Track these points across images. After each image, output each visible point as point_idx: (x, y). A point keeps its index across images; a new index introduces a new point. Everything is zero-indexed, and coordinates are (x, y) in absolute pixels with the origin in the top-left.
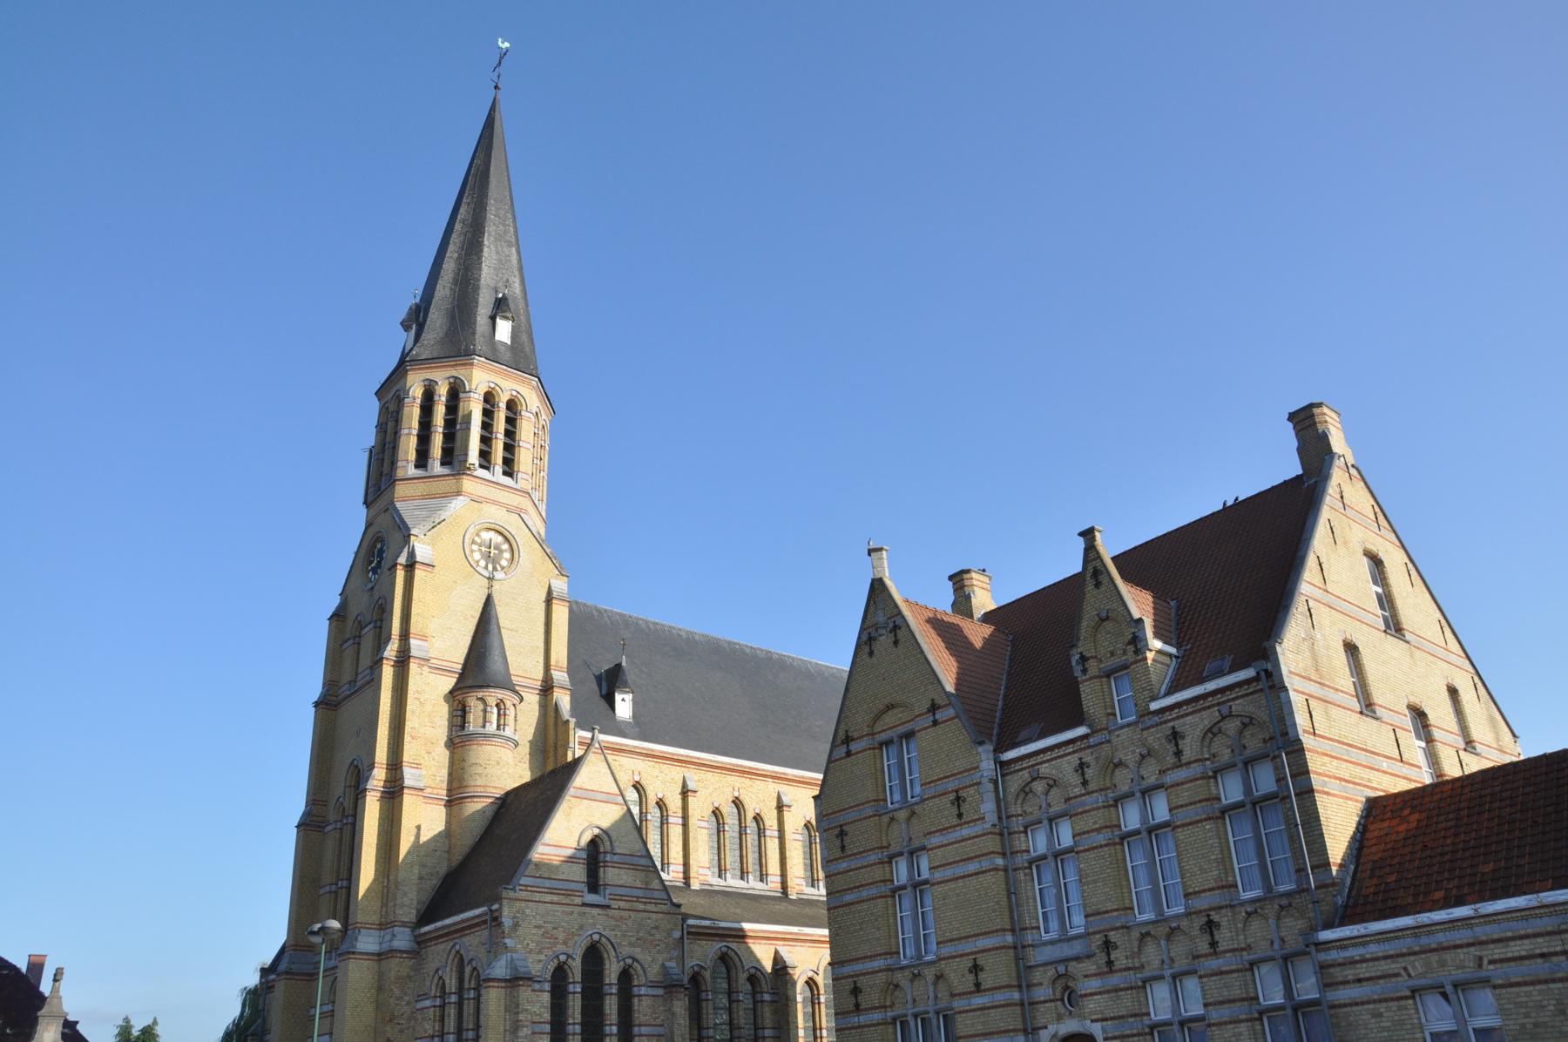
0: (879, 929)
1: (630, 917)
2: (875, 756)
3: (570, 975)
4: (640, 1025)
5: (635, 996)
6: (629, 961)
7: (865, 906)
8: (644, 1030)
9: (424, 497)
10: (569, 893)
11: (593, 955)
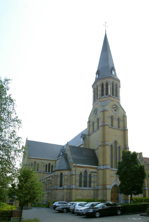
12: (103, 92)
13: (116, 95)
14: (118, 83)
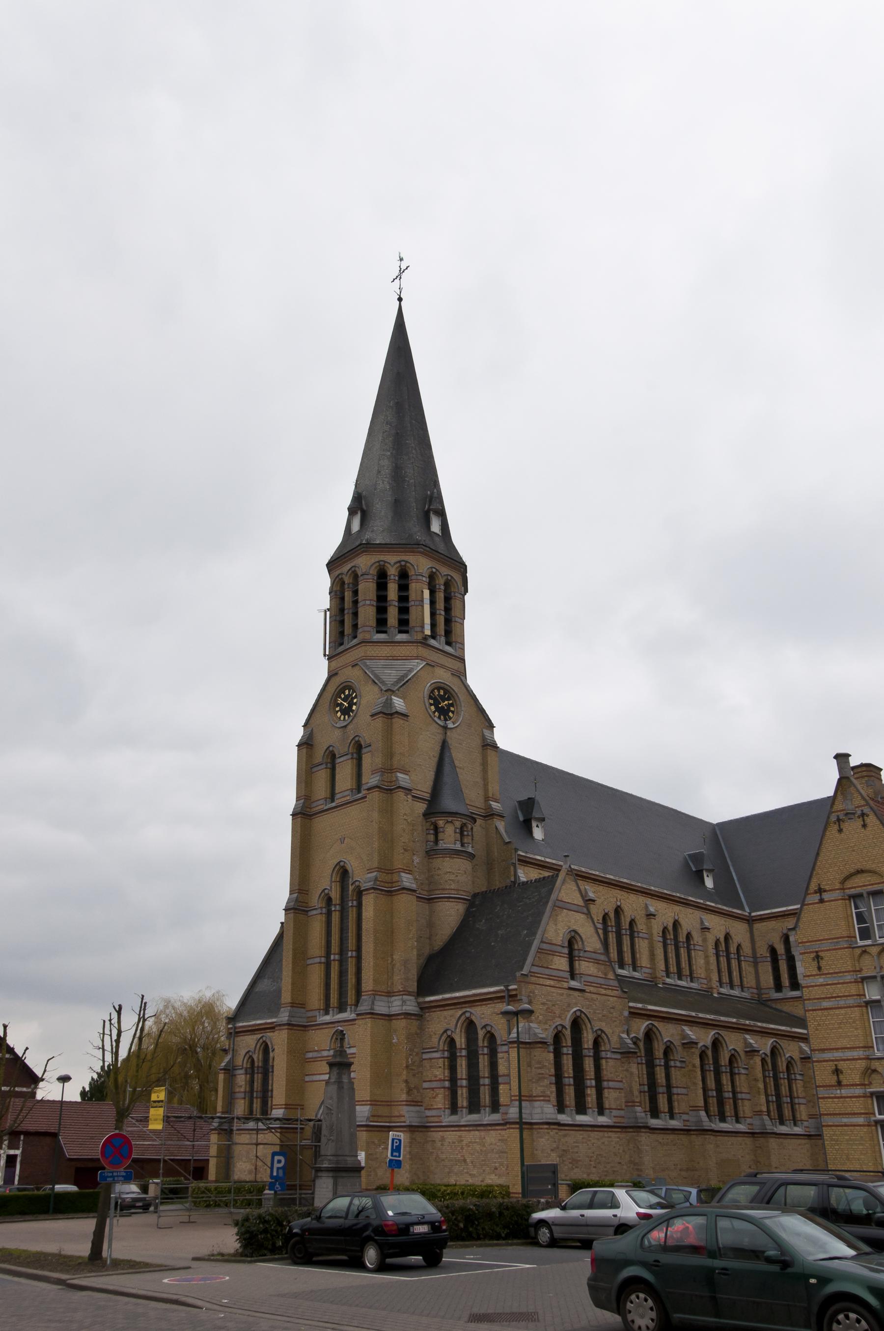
0: (856, 1029)
1: (597, 999)
2: (846, 905)
3: (564, 1041)
4: (608, 1081)
5: (603, 1058)
6: (599, 1032)
7: (843, 1011)
8: (611, 1084)
9: (387, 658)
10: (560, 979)
11: (576, 1024)
12: (381, 610)
13: (448, 633)
14: (457, 577)
